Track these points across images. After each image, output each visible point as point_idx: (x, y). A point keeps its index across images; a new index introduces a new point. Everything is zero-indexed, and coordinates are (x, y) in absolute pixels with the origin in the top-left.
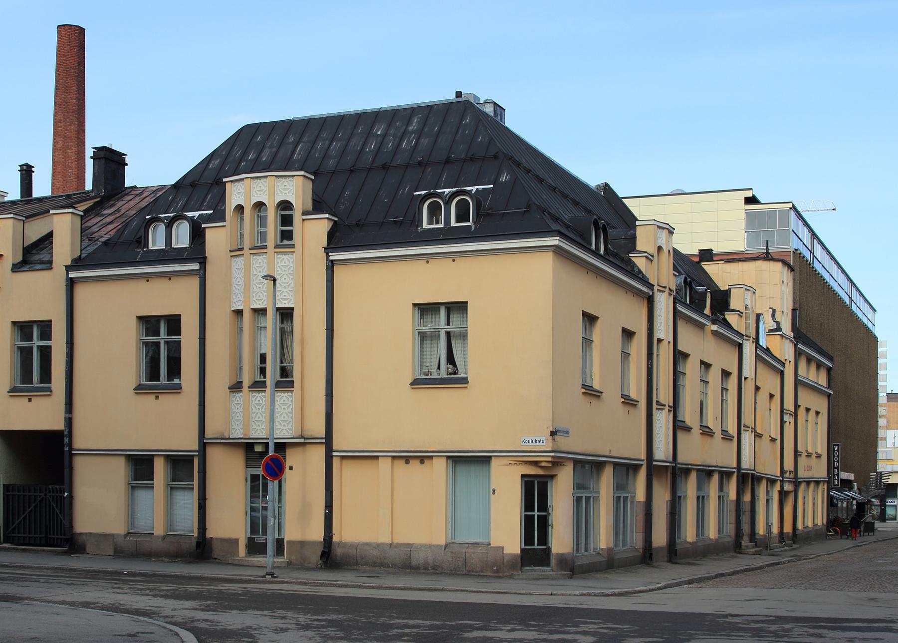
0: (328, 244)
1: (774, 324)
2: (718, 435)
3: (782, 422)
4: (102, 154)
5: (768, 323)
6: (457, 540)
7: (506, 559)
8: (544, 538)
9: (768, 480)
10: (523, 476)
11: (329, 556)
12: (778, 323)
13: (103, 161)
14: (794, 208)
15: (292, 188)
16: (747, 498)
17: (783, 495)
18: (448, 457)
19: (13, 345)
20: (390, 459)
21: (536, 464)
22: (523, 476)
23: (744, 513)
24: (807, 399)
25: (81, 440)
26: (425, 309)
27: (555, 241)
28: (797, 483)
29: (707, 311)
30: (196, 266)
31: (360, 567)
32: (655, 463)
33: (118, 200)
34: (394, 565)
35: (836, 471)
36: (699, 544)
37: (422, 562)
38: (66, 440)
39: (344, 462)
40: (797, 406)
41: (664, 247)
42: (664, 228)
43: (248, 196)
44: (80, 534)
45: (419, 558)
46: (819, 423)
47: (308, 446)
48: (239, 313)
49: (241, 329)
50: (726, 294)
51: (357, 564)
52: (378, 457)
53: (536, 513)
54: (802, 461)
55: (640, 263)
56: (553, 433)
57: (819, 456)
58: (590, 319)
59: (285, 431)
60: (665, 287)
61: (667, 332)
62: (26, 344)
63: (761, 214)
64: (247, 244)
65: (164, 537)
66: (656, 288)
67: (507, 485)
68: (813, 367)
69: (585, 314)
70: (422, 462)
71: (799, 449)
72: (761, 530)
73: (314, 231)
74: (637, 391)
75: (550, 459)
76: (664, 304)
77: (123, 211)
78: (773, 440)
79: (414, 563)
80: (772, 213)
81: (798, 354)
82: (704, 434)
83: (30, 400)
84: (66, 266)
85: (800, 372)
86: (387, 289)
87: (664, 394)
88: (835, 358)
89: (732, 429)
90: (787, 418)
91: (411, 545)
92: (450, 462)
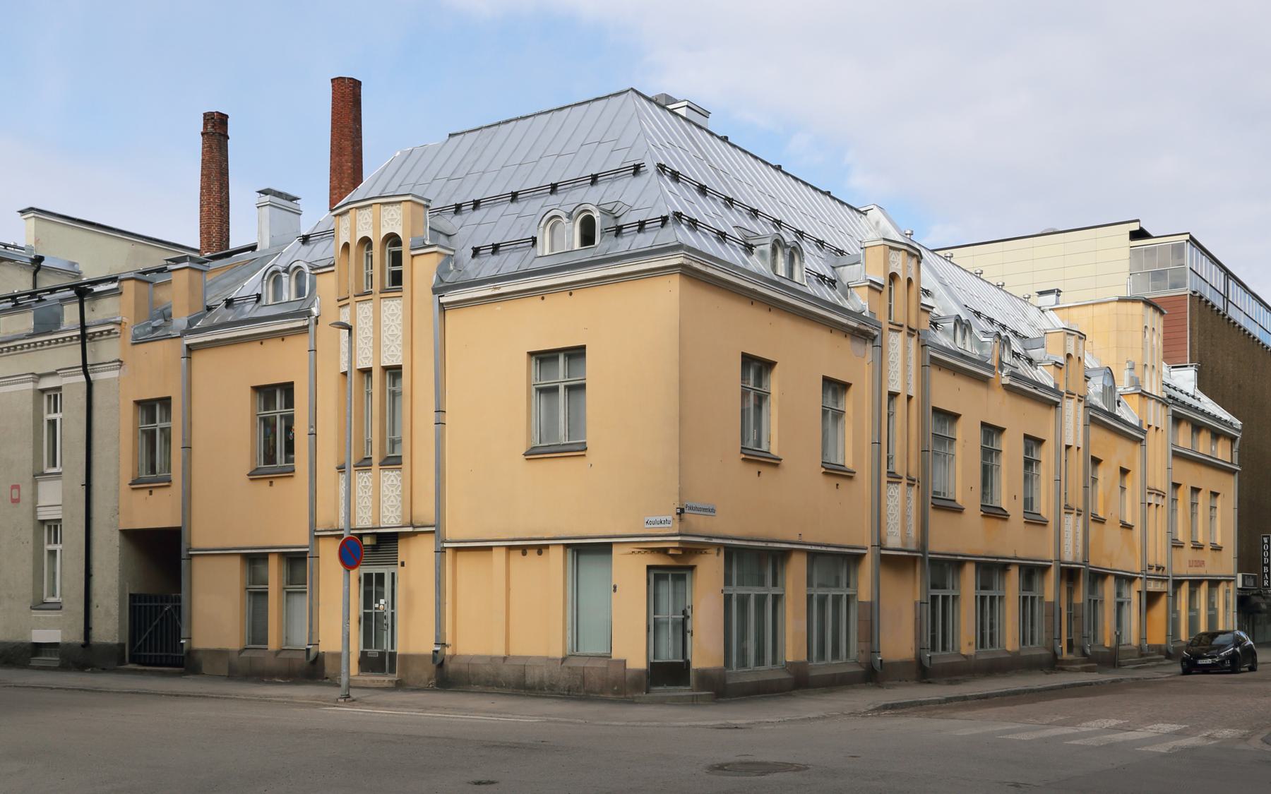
6: (582, 651)
7: (629, 675)
10: (649, 568)
14: (1193, 240)
18: (566, 546)
19: (135, 429)
20: (504, 550)
21: (664, 551)
22: (649, 568)
23: (937, 613)
25: (200, 537)
26: (543, 358)
34: (508, 685)
35: (1266, 569)
36: (1022, 654)
37: (537, 680)
39: (459, 554)
41: (900, 274)
42: (900, 250)
43: (377, 225)
44: (197, 651)
45: (533, 676)
46: (1219, 506)
47: (420, 537)
49: (369, 394)
51: (469, 683)
52: (490, 548)
56: (681, 512)
57: (1217, 549)
59: (391, 520)
62: (150, 426)
63: (1151, 252)
64: (376, 287)
65: (277, 653)
67: (629, 572)
69: (747, 360)
70: (540, 553)
75: (677, 545)
79: (529, 681)
80: (1163, 248)
83: (151, 493)
92: (569, 551)
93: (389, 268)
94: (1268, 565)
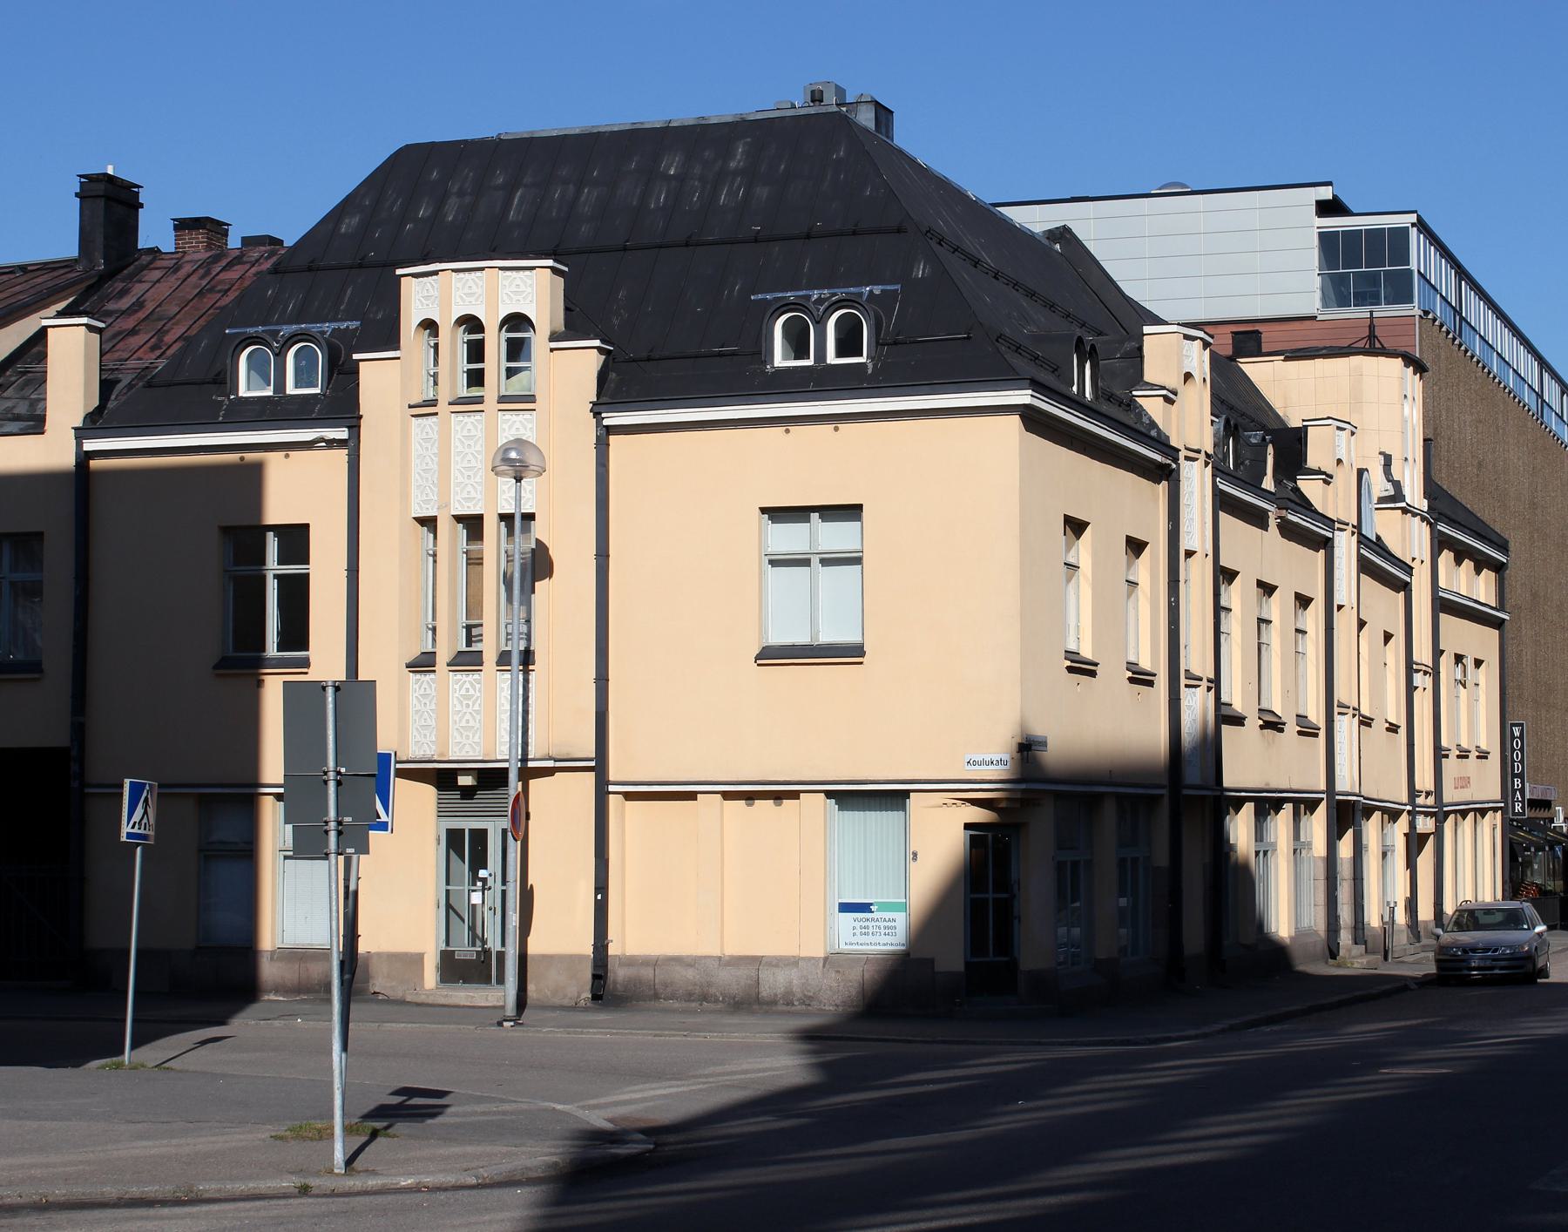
0: (598, 396)
1: (1389, 486)
2: (1292, 728)
3: (1411, 689)
4: (100, 188)
5: (1378, 485)
8: (1005, 941)
9: (1384, 810)
11: (607, 986)
12: (1397, 485)
13: (101, 202)
14: (1421, 225)
15: (529, 288)
16: (1345, 848)
17: (1415, 842)
22: (967, 826)
24: (1459, 634)
27: (1023, 397)
28: (1440, 816)
29: (1268, 483)
30: (343, 434)
31: (663, 1003)
32: (1186, 792)
33: (131, 277)
35: (1517, 782)
37: (780, 990)
38: (74, 767)
40: (1437, 653)
48: (429, 523)
50: (1300, 436)
51: (656, 996)
53: (991, 896)
54: (1450, 765)
55: (1152, 406)
57: (1483, 756)
58: (1076, 527)
59: (500, 750)
60: (1198, 451)
61: (1203, 541)
63: (1352, 236)
64: (444, 396)
66: (1182, 455)
68: (1468, 565)
71: (1444, 743)
72: (1373, 918)
73: (570, 372)
74: (1151, 656)
76: (1196, 481)
77: (150, 307)
78: (1393, 728)
79: (765, 992)
81: (1440, 543)
82: (1267, 725)
84: (76, 429)
85: (1442, 583)
86: (708, 475)
87: (1196, 658)
88: (1515, 560)
89: (1316, 716)
90: (1418, 679)
91: (756, 961)
93: (463, 365)
94: (1521, 776)
